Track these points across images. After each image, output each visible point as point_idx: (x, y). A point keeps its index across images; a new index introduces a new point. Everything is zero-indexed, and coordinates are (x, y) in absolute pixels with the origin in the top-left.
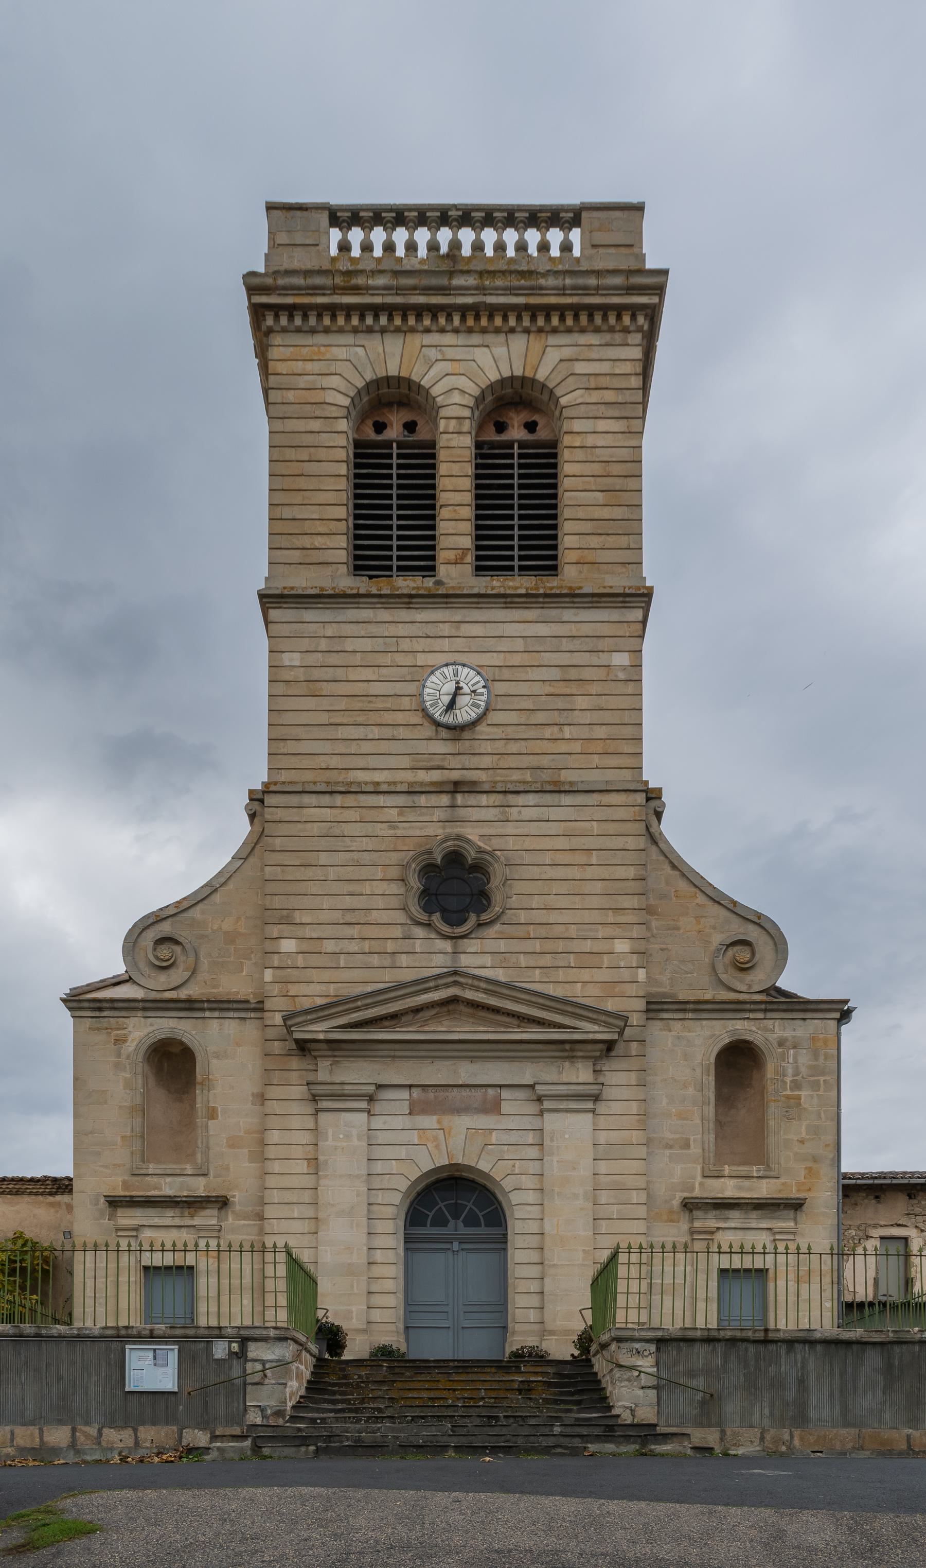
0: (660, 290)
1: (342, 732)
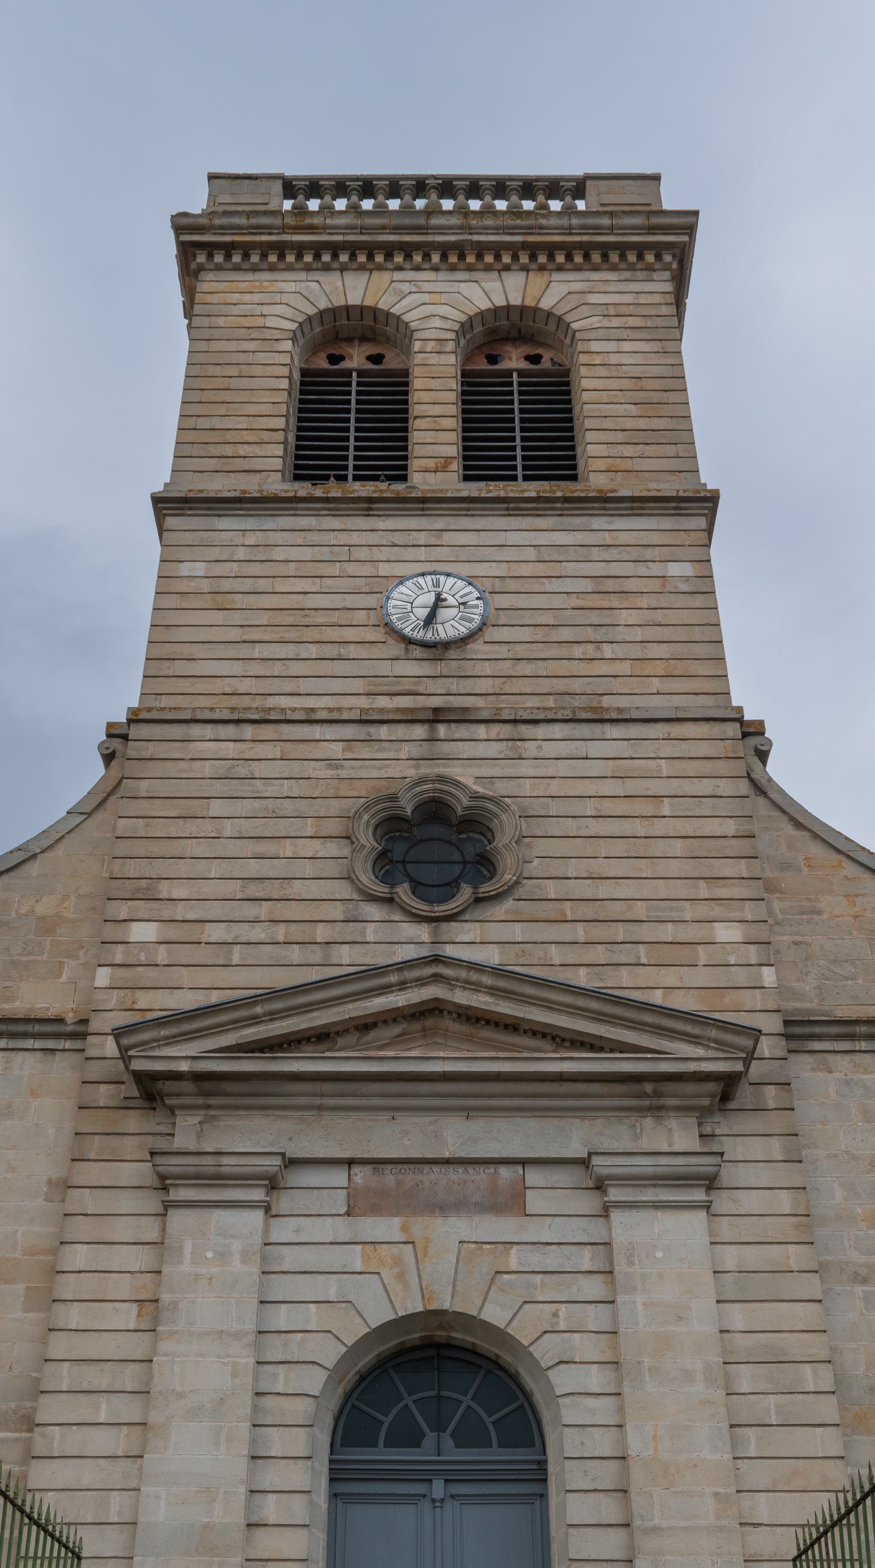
0: (690, 230)
1: (258, 651)
